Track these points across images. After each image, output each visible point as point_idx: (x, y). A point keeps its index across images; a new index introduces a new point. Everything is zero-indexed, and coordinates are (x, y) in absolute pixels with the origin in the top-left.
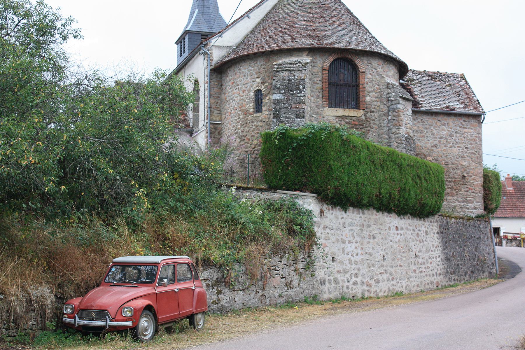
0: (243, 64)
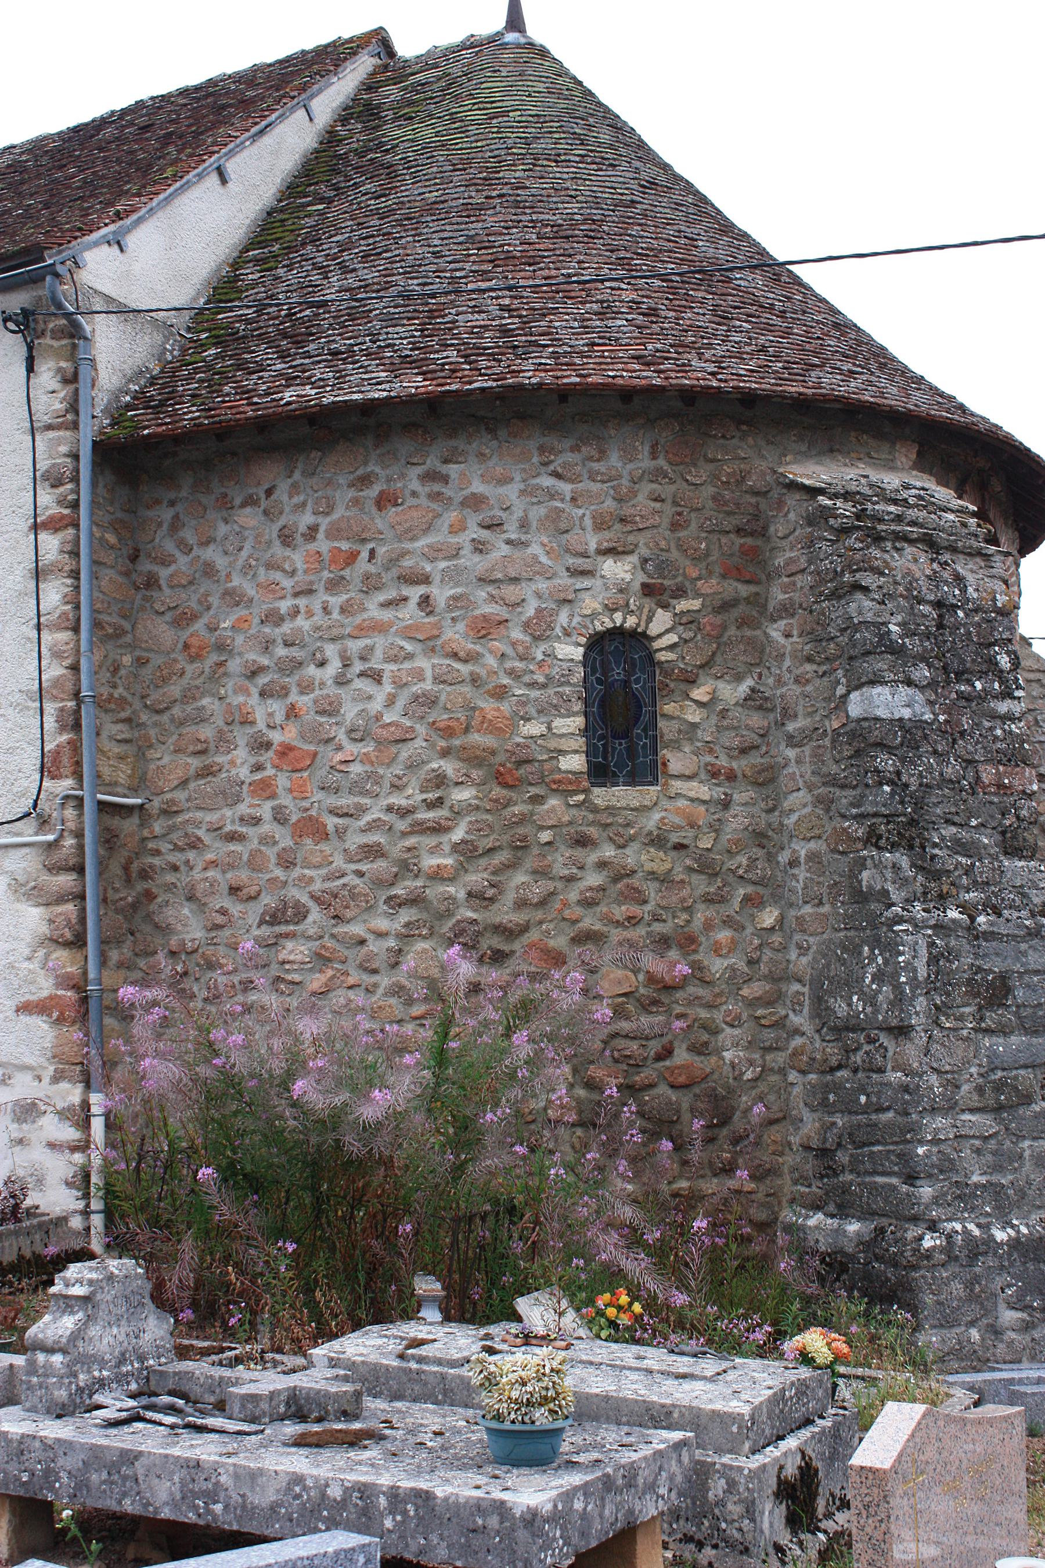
0: (482, 443)
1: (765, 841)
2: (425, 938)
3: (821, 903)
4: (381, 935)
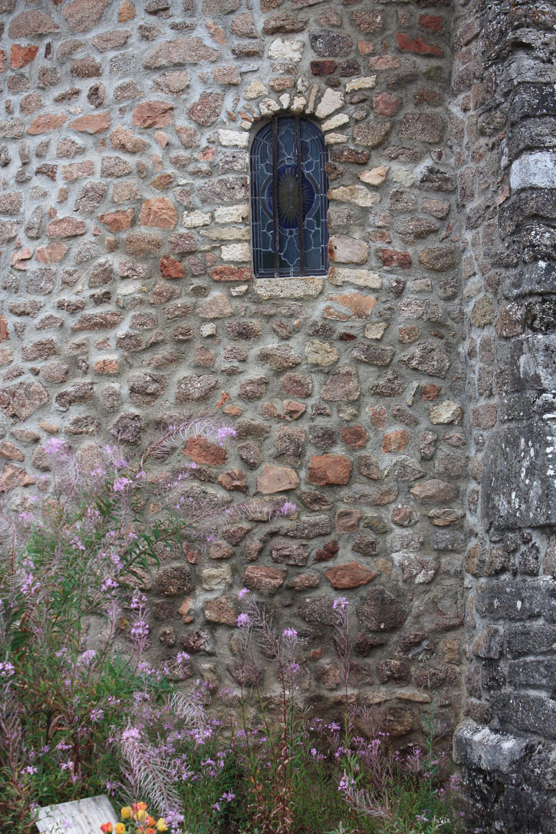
1: (443, 331)
2: (92, 434)
3: (491, 395)
4: (53, 433)
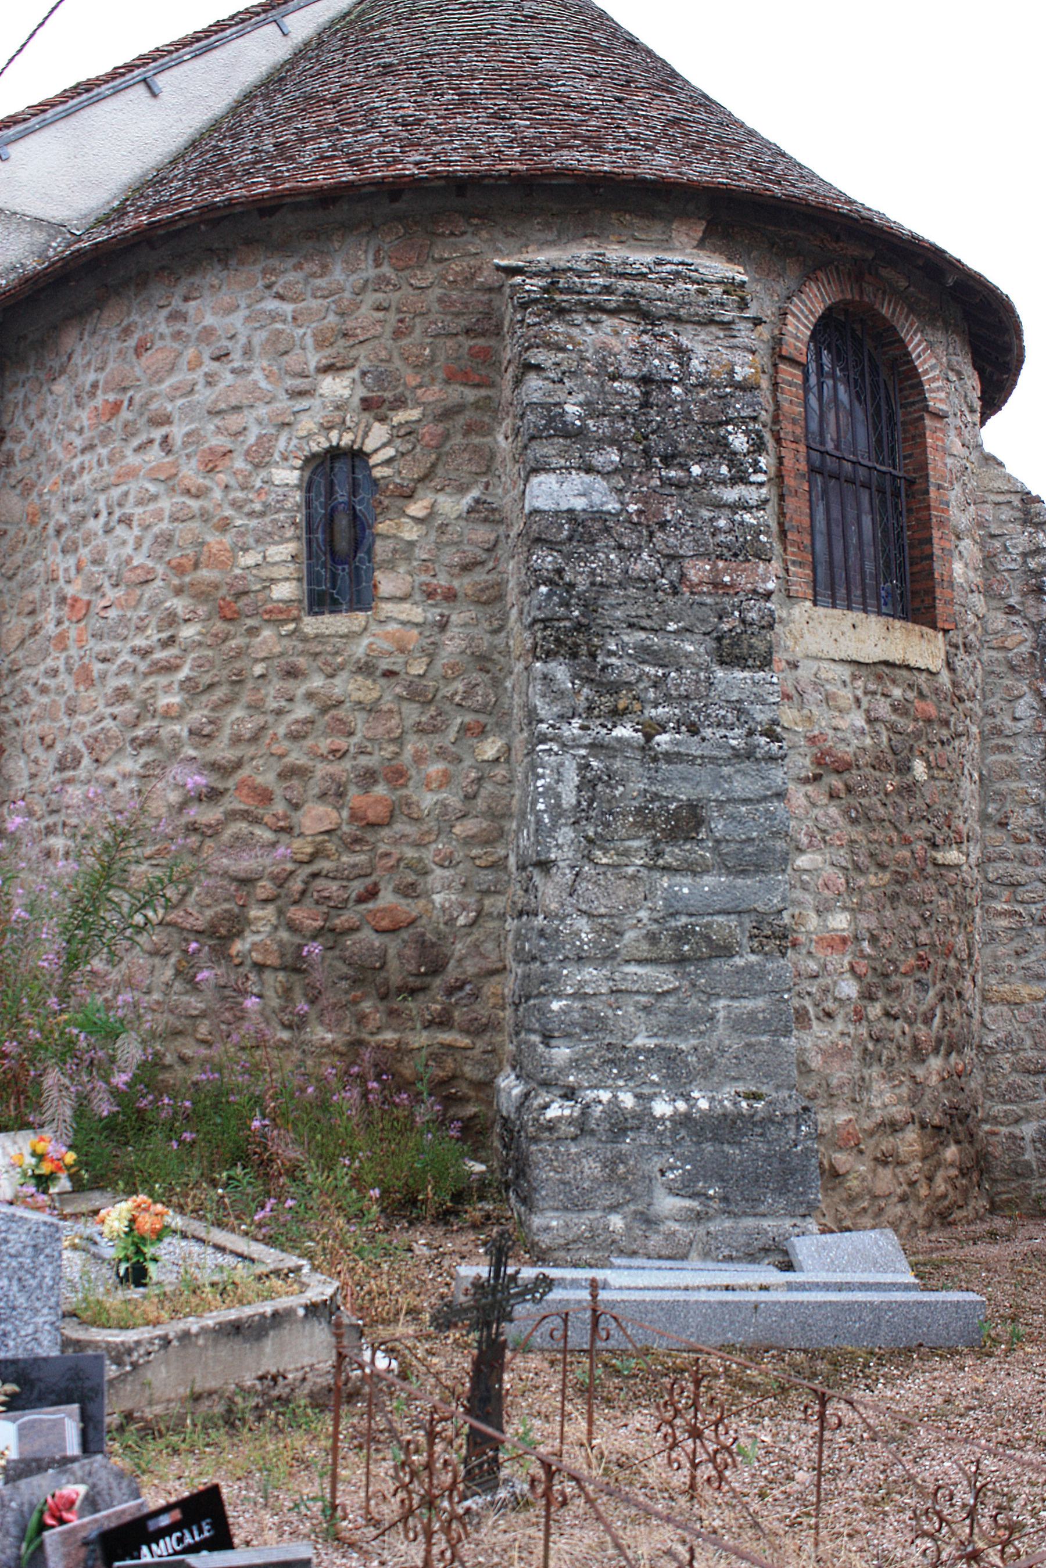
0: (212, 277)
1: (489, 665)
4: (126, 776)
